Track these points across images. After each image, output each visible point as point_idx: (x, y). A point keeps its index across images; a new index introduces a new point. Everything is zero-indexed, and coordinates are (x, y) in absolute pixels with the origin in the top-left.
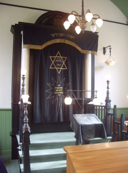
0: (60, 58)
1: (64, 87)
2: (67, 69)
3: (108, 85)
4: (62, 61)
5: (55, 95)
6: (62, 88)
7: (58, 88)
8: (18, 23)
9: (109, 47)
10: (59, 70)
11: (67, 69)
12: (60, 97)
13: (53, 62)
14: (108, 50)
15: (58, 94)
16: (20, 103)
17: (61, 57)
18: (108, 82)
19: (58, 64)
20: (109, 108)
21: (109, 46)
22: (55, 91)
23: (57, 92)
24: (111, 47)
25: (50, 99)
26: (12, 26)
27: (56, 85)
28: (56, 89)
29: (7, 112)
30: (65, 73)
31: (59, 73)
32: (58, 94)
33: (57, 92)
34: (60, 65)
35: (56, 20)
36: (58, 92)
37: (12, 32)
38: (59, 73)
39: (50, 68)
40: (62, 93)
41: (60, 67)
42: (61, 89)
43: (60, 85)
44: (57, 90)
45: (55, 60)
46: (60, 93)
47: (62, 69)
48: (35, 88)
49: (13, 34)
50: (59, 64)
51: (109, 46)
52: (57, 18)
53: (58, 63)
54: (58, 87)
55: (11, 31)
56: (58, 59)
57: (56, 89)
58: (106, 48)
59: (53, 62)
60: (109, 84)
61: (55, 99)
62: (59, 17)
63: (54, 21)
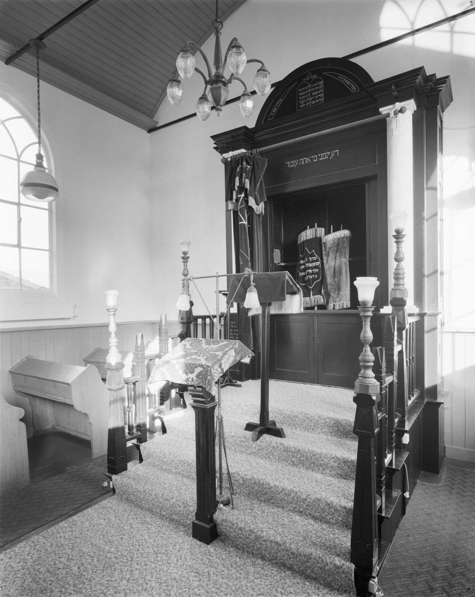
63: (299, 96)
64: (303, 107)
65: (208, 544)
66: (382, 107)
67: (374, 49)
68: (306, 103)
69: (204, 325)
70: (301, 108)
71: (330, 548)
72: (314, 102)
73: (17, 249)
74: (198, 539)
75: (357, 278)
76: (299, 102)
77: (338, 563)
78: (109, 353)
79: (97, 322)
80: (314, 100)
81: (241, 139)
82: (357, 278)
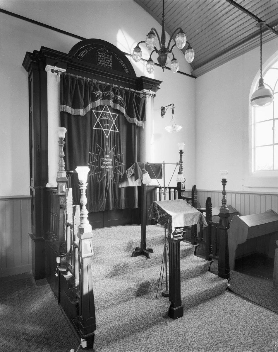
0: (108, 113)
1: (114, 158)
2: (118, 131)
3: (181, 157)
4: (111, 119)
5: (102, 170)
6: (111, 160)
7: (106, 159)
8: (39, 50)
9: (172, 106)
10: (107, 132)
11: (118, 131)
12: (108, 173)
13: (98, 120)
14: (168, 111)
15: (107, 169)
16: (188, 168)
17: (110, 113)
18: (181, 152)
19: (105, 123)
20: (183, 190)
21: (170, 105)
22: (102, 164)
23: (104, 165)
24: (174, 106)
25: (94, 176)
26: (28, 53)
27: (103, 156)
28: (104, 161)
29: (27, 201)
30: (116, 137)
31: (107, 137)
32: (107, 169)
33: (104, 165)
34: (109, 125)
35: (100, 54)
36: (107, 165)
37: (25, 68)
38: (107, 137)
39: (94, 128)
40: (111, 167)
41: (108, 128)
42: (110, 161)
43: (108, 156)
44: (104, 163)
45: (101, 117)
46: (109, 167)
47: (111, 131)
48: (104, 141)
49: (28, 71)
50: (108, 123)
51: (170, 105)
52: (103, 53)
53: (106, 122)
54: (107, 158)
55: (23, 65)
56: (106, 116)
57: (104, 161)
58: (166, 109)
59: (98, 120)
60: (182, 156)
61: (101, 176)
62: (105, 51)
63: (98, 56)
64: (100, 64)
65: (183, 316)
66: (49, 64)
67: (22, 19)
68: (102, 63)
69: (170, 192)
70: (99, 64)
71: (214, 280)
72: (107, 65)
73: (272, 143)
74: (178, 318)
75: (77, 167)
76: (98, 60)
77: (224, 282)
78: (89, 223)
79: (234, 190)
80: (106, 63)
81: (67, 62)
82: (77, 167)
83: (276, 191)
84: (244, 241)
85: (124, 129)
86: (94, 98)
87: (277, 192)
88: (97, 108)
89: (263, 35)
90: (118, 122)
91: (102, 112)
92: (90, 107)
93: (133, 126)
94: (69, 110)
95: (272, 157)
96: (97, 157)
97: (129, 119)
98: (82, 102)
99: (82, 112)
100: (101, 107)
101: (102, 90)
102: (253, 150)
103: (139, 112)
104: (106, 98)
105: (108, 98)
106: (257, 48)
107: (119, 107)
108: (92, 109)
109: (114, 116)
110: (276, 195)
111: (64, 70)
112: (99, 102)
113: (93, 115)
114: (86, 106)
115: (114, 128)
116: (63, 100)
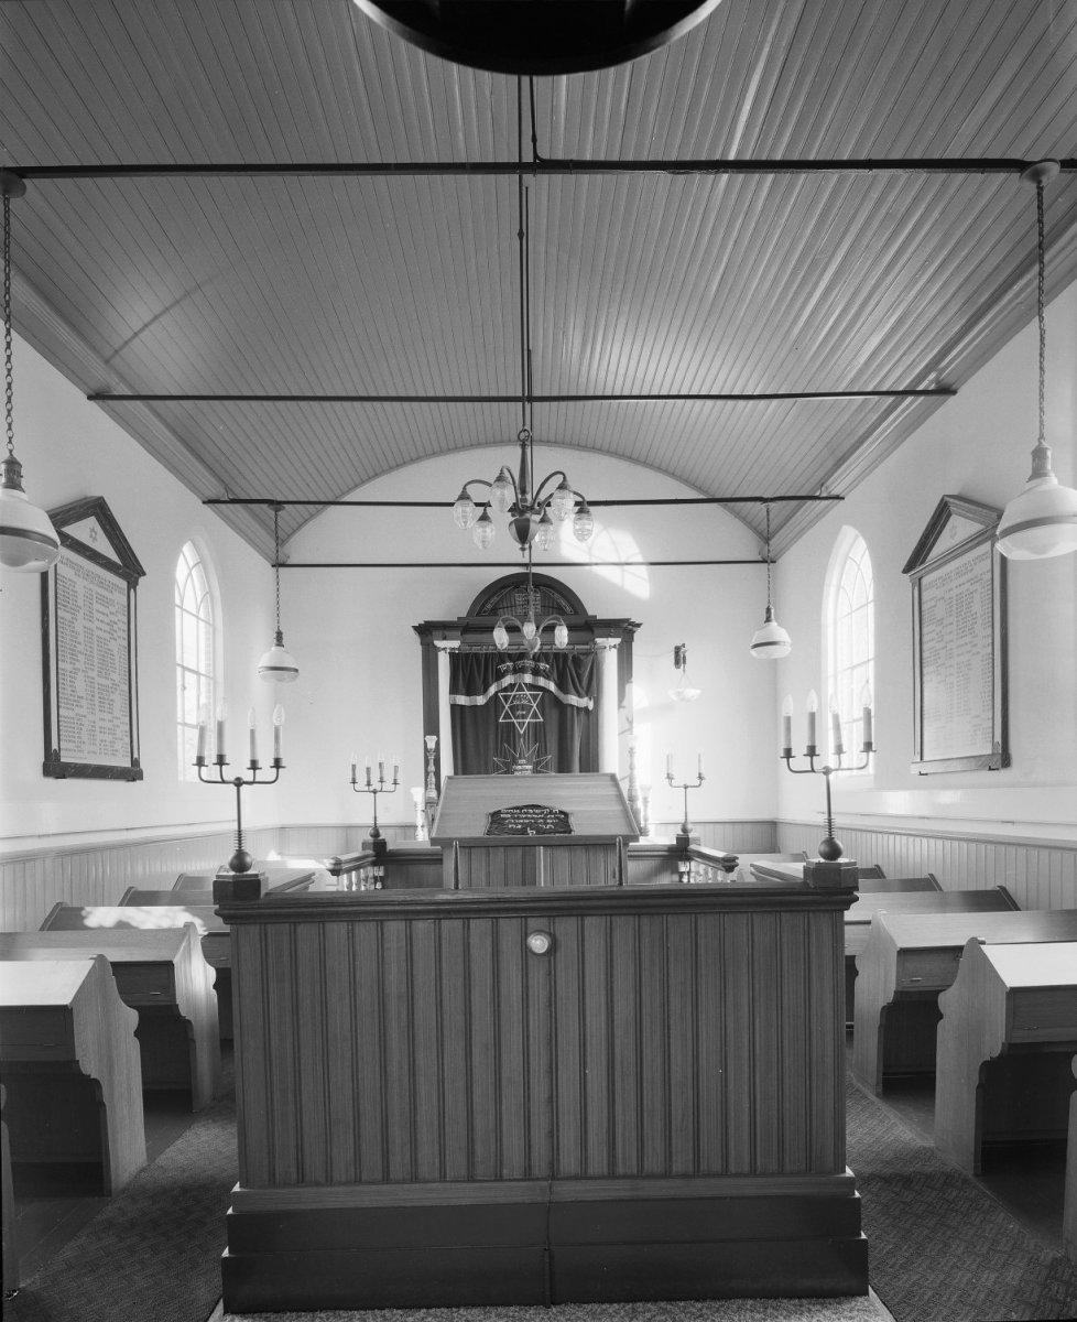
30: (538, 732)
41: (524, 717)
83: (1071, 836)
84: (996, 1053)
85: (554, 714)
86: (500, 676)
87: (1075, 838)
88: (505, 689)
89: (1051, 261)
90: (541, 706)
91: (513, 693)
92: (492, 690)
93: (569, 709)
94: (462, 700)
95: (426, 568)
96: (505, 764)
97: (561, 696)
98: (479, 682)
99: (481, 700)
100: (512, 686)
101: (511, 660)
102: (831, 681)
103: (580, 682)
104: (518, 671)
105: (522, 670)
106: (1019, 338)
107: (542, 682)
108: (497, 693)
109: (535, 697)
110: (1071, 849)
111: (456, 644)
112: (508, 680)
113: (514, 732)
114: (486, 690)
115: (535, 716)
116: (454, 690)
